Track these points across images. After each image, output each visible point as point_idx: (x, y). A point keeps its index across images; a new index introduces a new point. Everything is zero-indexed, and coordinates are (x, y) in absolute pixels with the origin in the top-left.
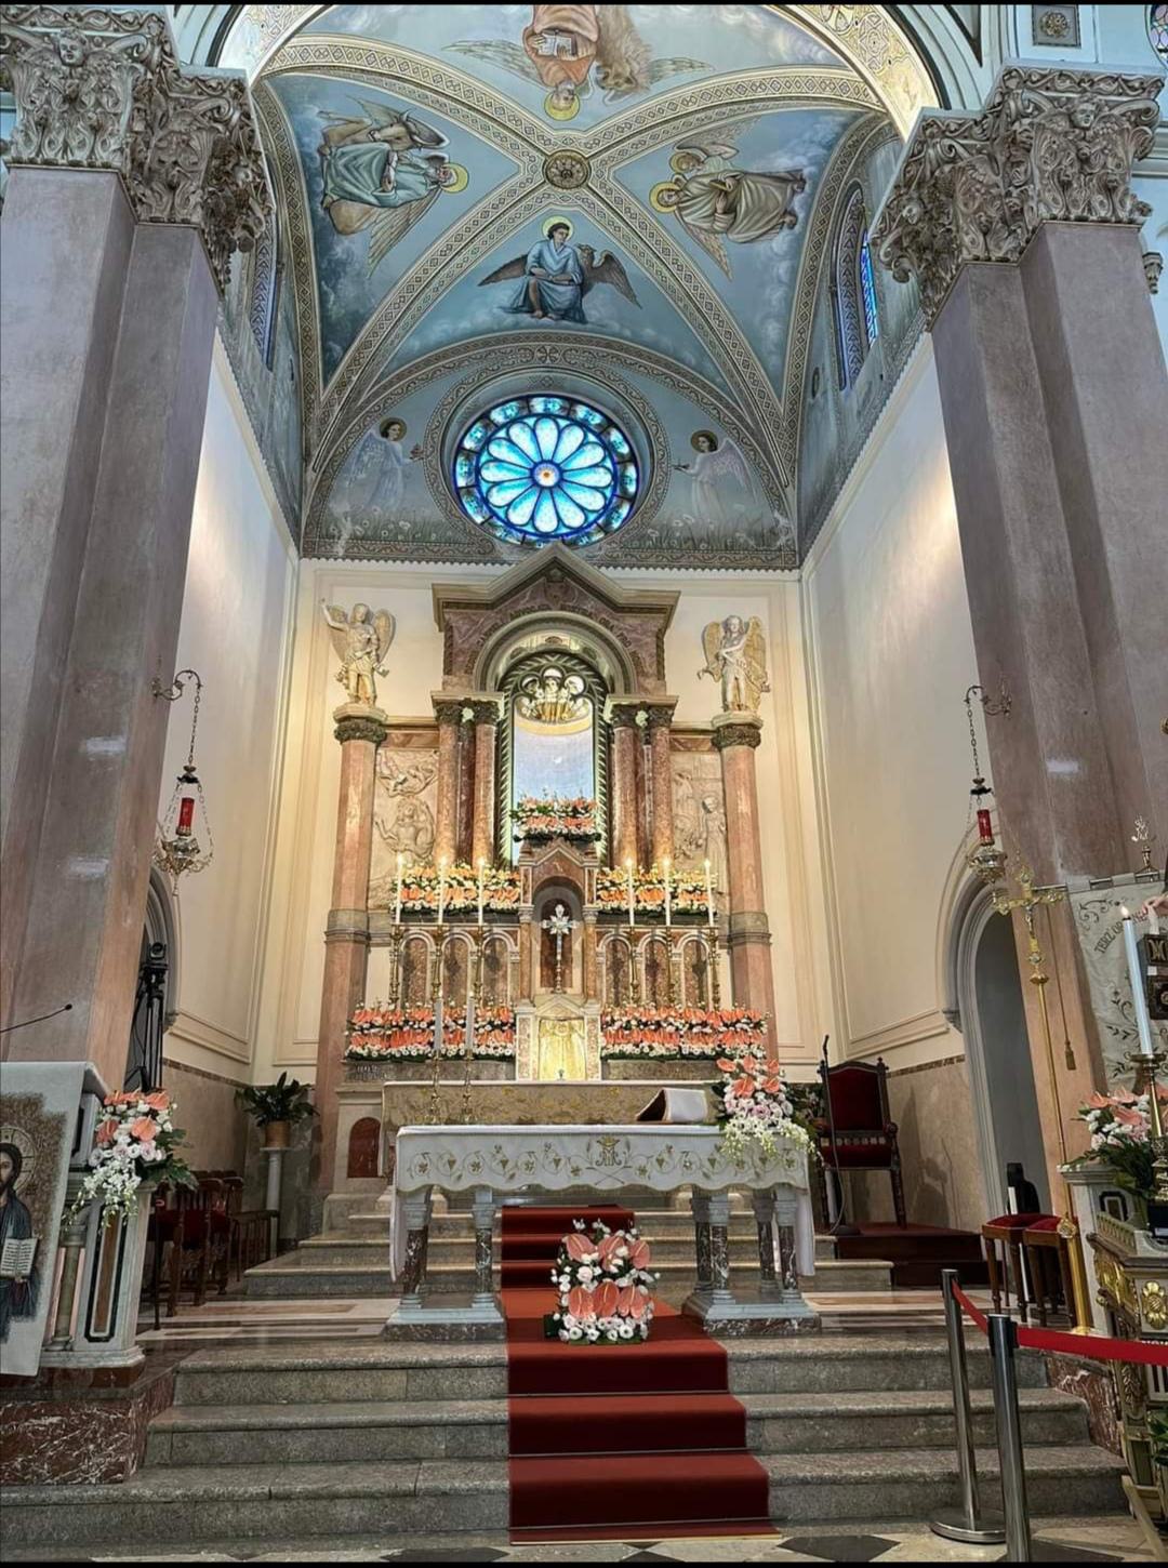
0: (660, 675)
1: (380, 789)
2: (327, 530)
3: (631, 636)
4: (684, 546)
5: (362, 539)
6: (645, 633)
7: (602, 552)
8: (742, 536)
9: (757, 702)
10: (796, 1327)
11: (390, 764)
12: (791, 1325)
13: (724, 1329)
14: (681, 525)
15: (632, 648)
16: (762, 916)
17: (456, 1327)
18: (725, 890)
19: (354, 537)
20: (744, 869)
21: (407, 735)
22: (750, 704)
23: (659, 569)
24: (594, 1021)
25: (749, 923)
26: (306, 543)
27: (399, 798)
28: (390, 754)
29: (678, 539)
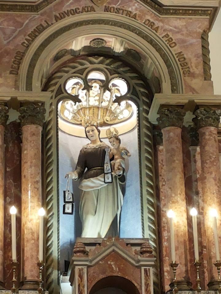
0: (207, 75)
3: (175, 37)
6: (190, 34)
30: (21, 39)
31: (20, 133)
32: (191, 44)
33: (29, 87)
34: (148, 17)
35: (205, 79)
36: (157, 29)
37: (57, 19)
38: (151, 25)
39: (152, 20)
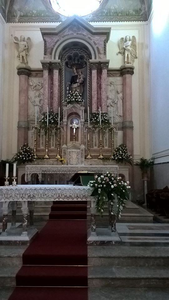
0: (105, 53)
1: (30, 89)
2: (13, 14)
3: (96, 42)
4: (114, 15)
5: (23, 16)
6: (100, 41)
7: (91, 17)
8: (131, 11)
9: (133, 61)
10: (114, 243)
11: (32, 82)
12: (112, 243)
13: (93, 243)
14: (113, 8)
15: (97, 46)
16: (131, 122)
17: (16, 242)
18: (122, 115)
19: (21, 16)
20: (127, 109)
21: (36, 73)
22: (131, 62)
23: (107, 22)
24: (83, 150)
25: (128, 124)
26: (7, 18)
27: (35, 91)
28: (32, 79)
29: (113, 13)
30: (53, 44)
31: (25, 210)
32: (101, 44)
33: (55, 58)
34: (89, 36)
35: (104, 55)
36: (91, 40)
37: (63, 37)
38: (89, 38)
39: (90, 37)
